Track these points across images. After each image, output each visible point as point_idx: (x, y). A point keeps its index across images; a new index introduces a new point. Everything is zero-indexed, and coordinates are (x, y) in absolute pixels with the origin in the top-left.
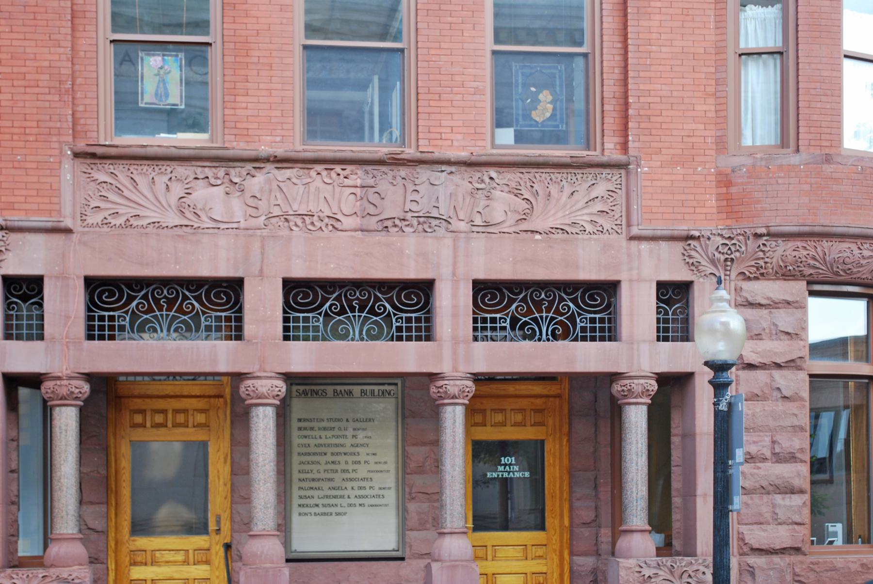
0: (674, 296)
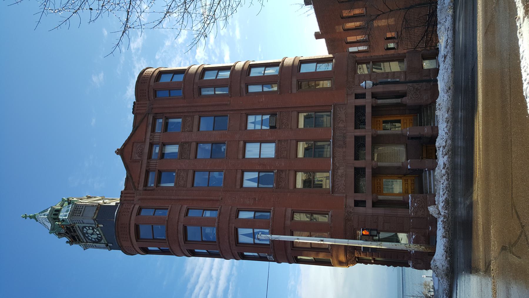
0: (357, 96)
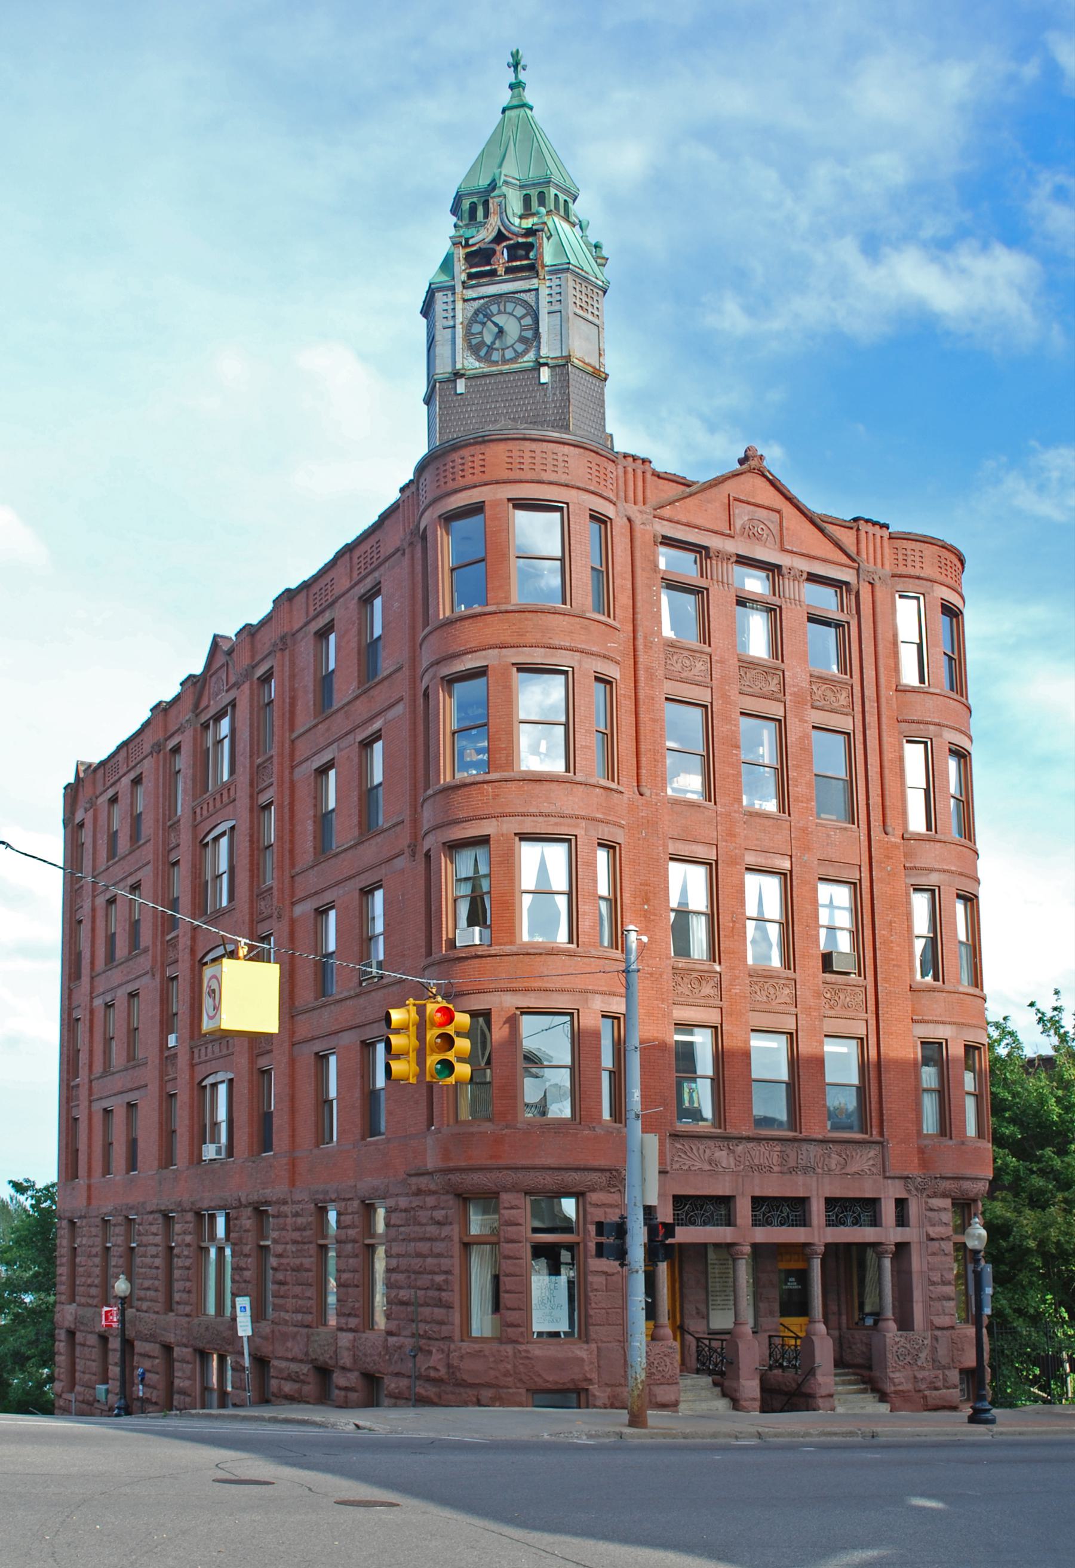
0: (901, 1204)
